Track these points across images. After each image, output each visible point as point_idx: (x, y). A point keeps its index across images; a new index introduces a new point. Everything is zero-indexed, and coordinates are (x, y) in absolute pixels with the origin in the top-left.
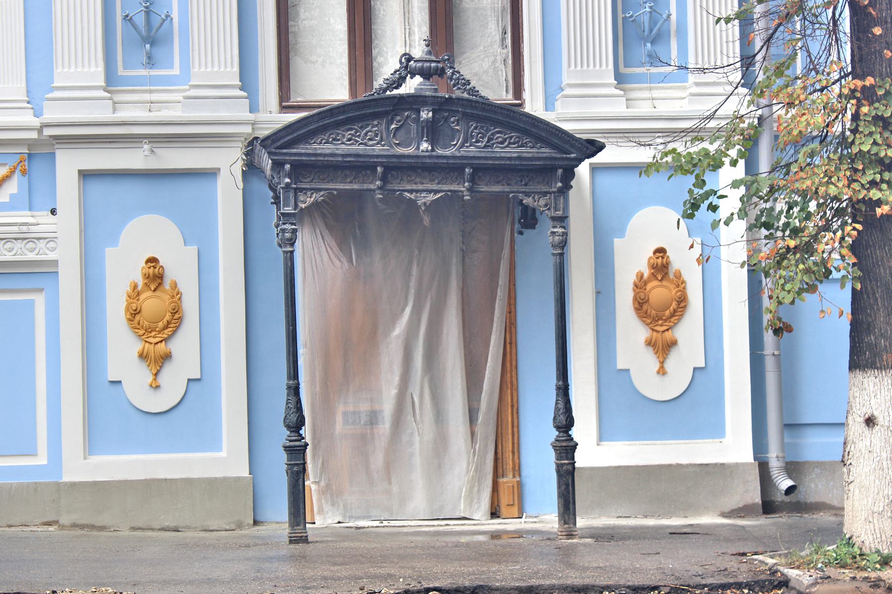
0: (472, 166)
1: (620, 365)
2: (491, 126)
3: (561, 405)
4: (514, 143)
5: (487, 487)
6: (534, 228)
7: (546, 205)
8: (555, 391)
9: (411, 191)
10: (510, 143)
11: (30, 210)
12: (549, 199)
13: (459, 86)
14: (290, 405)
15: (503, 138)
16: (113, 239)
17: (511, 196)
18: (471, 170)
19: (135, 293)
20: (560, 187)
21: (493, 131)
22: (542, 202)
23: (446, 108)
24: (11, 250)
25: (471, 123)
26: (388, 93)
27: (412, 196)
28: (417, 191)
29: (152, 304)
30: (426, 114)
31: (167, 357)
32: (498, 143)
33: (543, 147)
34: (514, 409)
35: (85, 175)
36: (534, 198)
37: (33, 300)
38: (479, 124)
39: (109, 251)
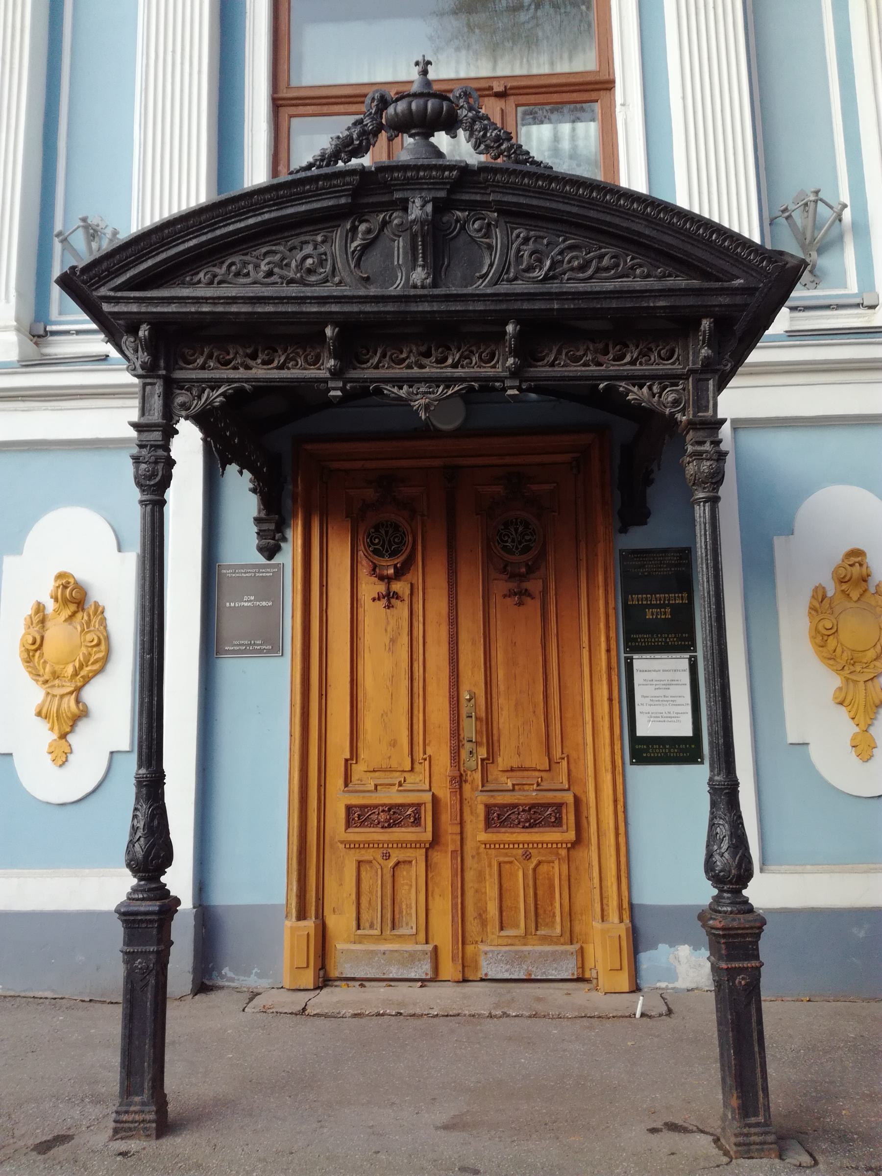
0: (519, 317)
2: (559, 236)
3: (723, 830)
4: (607, 269)
5: (705, 331)
6: (646, 523)
7: (676, 402)
8: (708, 795)
9: (399, 382)
10: (598, 270)
12: (684, 389)
13: (488, 142)
14: (138, 813)
15: (584, 259)
17: (601, 386)
18: (518, 327)
20: (706, 358)
21: (562, 246)
22: (670, 396)
23: (466, 197)
25: (516, 232)
27: (403, 392)
28: (411, 381)
31: (82, 714)
32: (572, 269)
33: (670, 275)
34: (619, 807)
36: (650, 388)
37: (702, 763)
38: (532, 233)
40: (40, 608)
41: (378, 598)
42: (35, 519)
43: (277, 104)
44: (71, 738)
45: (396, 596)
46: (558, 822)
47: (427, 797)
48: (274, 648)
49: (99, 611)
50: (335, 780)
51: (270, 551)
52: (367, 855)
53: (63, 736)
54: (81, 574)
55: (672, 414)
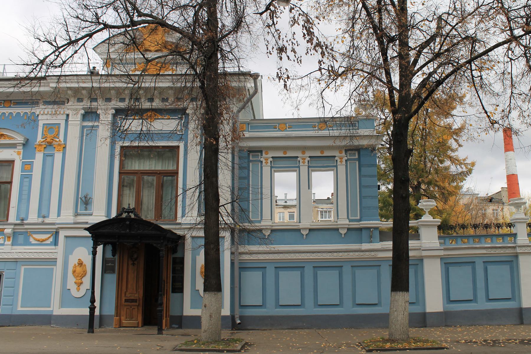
1: (68, 288)
11: (55, 245)
16: (71, 253)
19: (75, 266)
24: (23, 255)
26: (118, 217)
29: (79, 269)
30: (128, 223)
31: (81, 283)
35: (66, 237)
39: (70, 256)
40: (75, 265)
41: (132, 264)
42: (75, 249)
43: (120, 173)
44: (80, 287)
45: (135, 264)
46: (136, 302)
47: (138, 298)
48: (114, 272)
49: (85, 265)
50: (123, 295)
51: (114, 255)
52: (128, 307)
53: (79, 286)
54: (82, 260)
55: (151, 14)
